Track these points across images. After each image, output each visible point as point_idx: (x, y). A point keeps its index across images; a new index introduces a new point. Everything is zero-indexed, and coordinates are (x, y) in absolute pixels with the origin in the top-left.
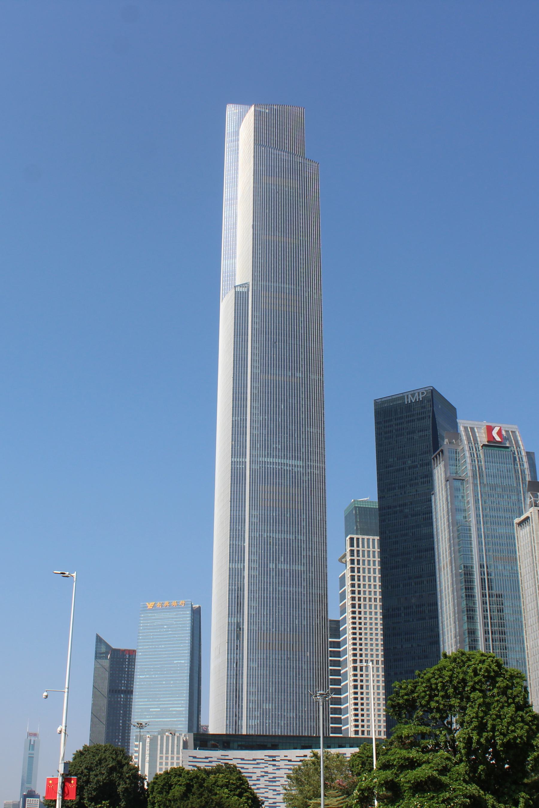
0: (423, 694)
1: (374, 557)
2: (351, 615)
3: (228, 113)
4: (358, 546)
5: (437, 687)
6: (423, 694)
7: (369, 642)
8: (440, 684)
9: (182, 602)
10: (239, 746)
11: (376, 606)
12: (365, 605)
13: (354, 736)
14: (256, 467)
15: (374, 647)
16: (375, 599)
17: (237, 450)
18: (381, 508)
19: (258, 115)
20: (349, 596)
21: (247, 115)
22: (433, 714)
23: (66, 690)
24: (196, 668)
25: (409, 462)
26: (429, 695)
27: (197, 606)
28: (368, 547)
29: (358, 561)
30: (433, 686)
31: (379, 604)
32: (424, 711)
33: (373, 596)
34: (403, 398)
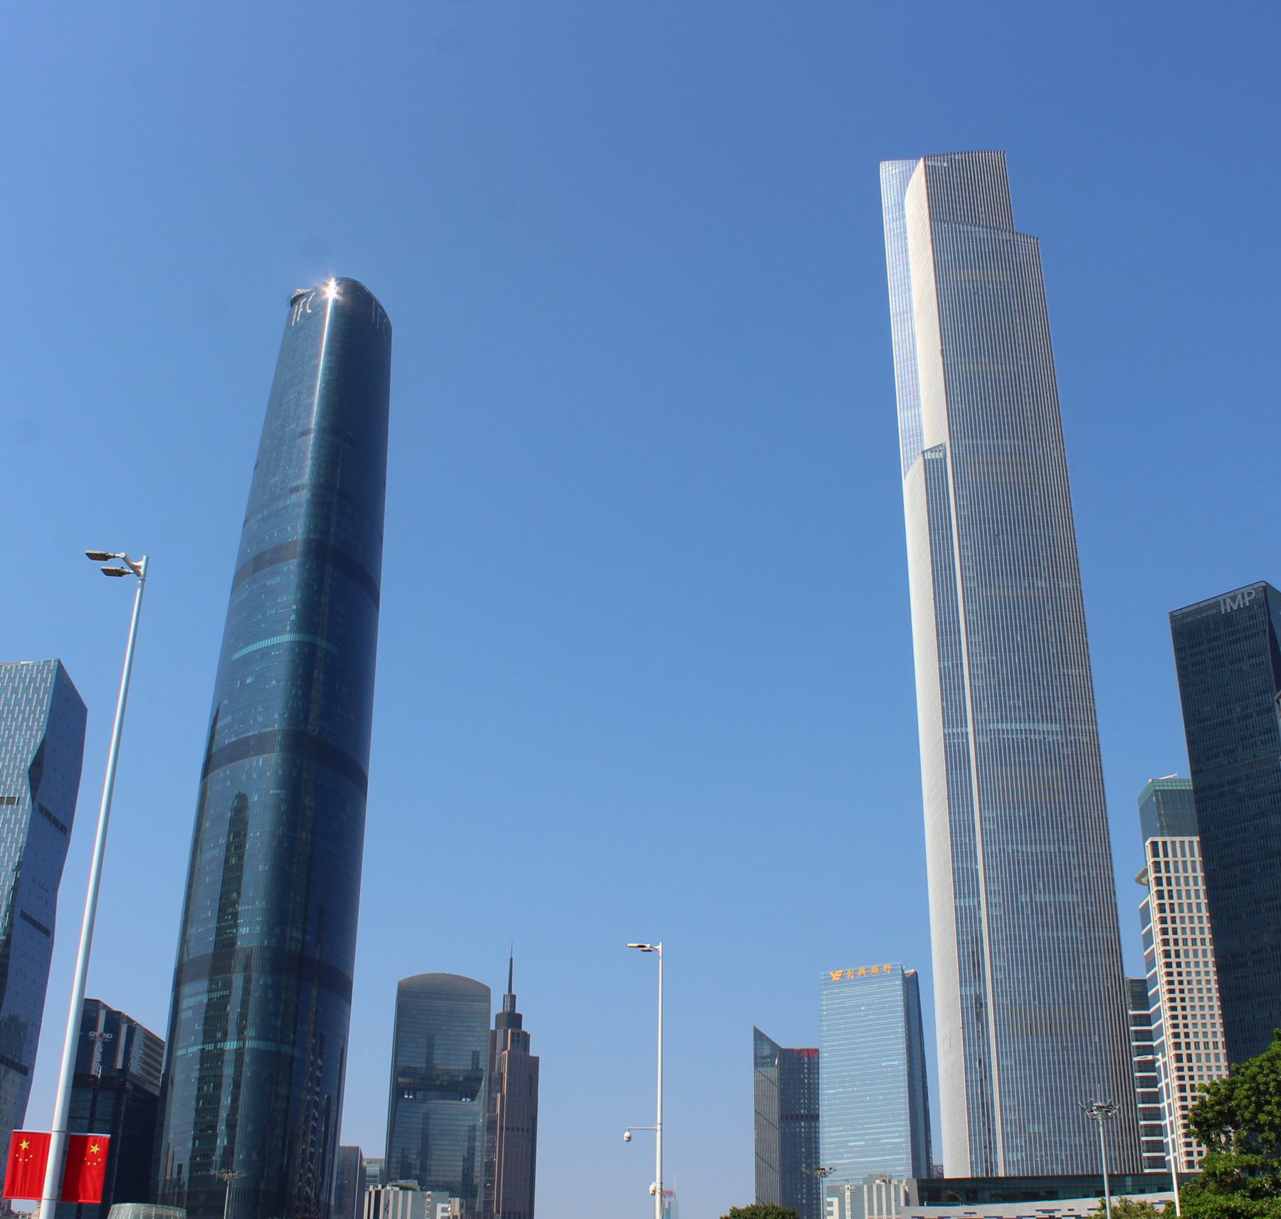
0: (1245, 1102)
1: (1194, 870)
2: (1165, 970)
3: (883, 175)
4: (1166, 855)
5: (1268, 1088)
6: (1245, 1102)
7: (1198, 1012)
8: (1272, 1084)
9: (886, 966)
10: (992, 1196)
11: (1204, 951)
12: (1186, 952)
13: (1186, 1171)
14: (983, 739)
15: (1208, 1020)
16: (1203, 941)
17: (952, 715)
18: (1198, 790)
19: (930, 173)
20: (1158, 938)
21: (914, 176)
22: (1265, 1135)
23: (659, 1127)
24: (918, 1073)
25: (1238, 709)
26: (1256, 1102)
27: (912, 971)
28: (1183, 855)
29: (1169, 879)
30: (1262, 1088)
31: (1209, 947)
32: (1250, 1129)
33: (1198, 936)
34: (1217, 605)
